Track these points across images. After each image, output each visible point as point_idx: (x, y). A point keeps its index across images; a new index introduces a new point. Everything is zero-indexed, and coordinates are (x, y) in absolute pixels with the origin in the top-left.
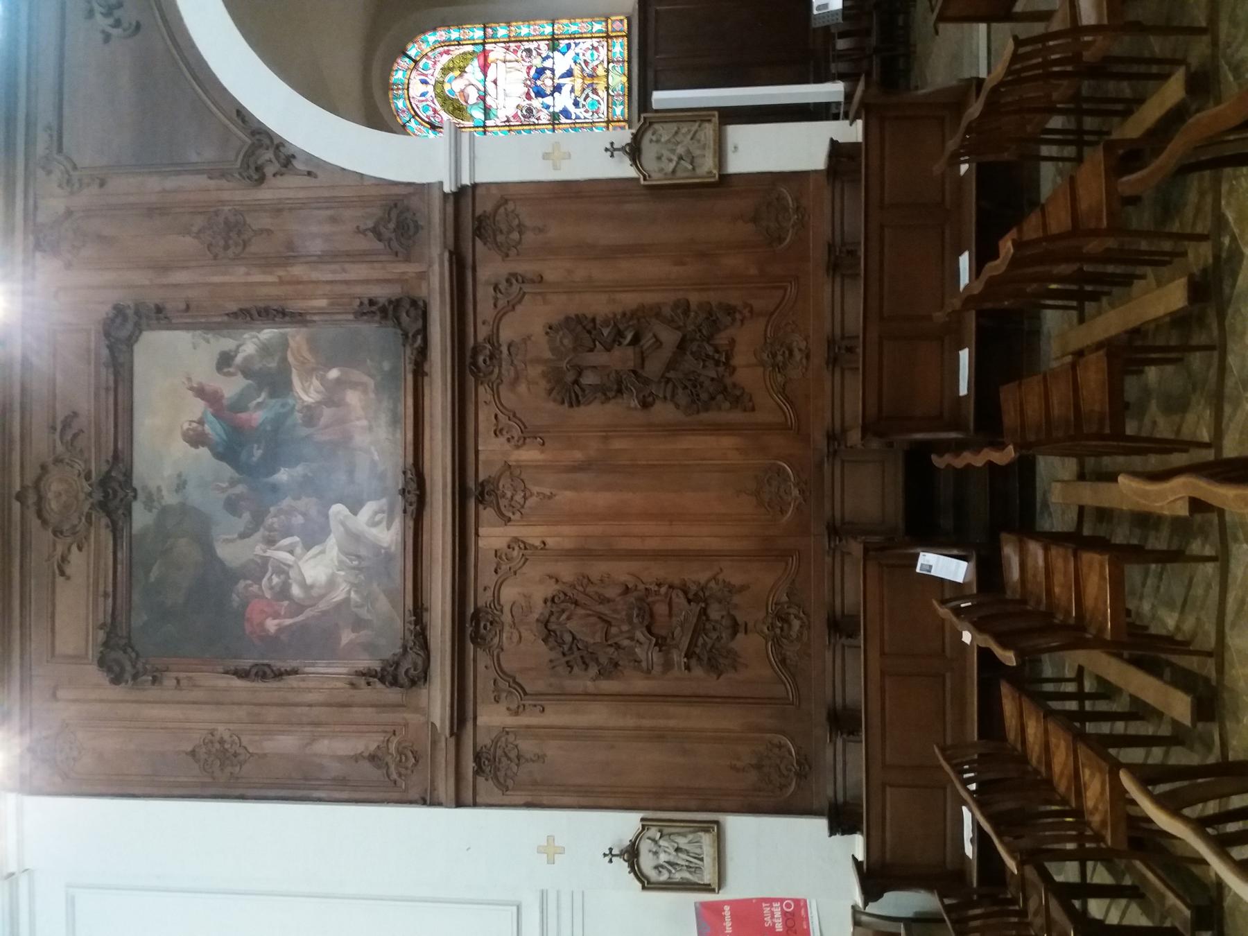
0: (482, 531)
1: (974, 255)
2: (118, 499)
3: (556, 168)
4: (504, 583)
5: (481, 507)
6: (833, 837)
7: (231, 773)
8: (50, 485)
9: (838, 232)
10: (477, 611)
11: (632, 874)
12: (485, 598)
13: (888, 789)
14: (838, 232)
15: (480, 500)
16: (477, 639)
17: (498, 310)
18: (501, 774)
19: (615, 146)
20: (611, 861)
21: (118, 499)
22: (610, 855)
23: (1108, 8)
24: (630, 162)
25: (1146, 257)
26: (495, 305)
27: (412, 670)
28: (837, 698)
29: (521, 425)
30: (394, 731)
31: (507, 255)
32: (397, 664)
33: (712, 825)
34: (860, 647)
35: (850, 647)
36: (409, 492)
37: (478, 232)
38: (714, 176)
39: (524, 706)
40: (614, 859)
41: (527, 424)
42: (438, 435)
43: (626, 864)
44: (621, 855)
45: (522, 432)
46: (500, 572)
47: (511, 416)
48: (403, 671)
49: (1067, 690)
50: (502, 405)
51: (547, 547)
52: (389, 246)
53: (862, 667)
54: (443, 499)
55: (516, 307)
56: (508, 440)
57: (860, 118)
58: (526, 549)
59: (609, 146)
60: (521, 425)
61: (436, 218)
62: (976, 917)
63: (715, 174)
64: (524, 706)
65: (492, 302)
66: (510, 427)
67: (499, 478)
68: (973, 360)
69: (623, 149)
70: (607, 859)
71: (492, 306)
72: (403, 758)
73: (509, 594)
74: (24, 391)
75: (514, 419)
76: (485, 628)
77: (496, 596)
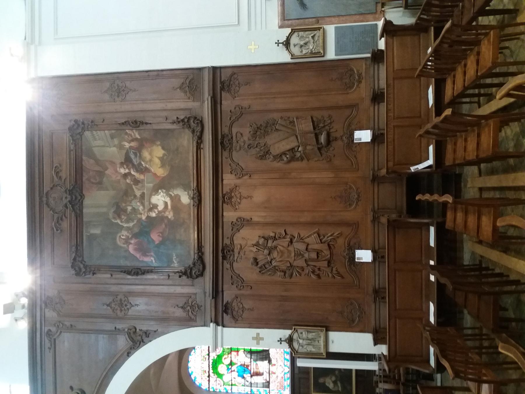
0: (225, 214)
1: (434, 145)
2: (78, 201)
3: (258, 334)
4: (234, 123)
5: (223, 151)
6: (376, 346)
7: (125, 313)
8: (51, 195)
9: (377, 306)
10: (223, 137)
11: (290, 349)
12: (227, 242)
13: (397, 272)
14: (377, 306)
15: (224, 148)
16: (224, 148)
17: (231, 121)
18: (232, 92)
19: (279, 42)
20: (281, 343)
21: (78, 201)
22: (278, 43)
23: (493, 220)
24: (286, 49)
25: (504, 38)
26: (232, 230)
27: (197, 272)
28: (375, 167)
29: (242, 280)
30: (191, 296)
31: (237, 320)
32: (191, 269)
33: (323, 329)
34: (386, 302)
35: (383, 302)
36: (195, 198)
37: (222, 89)
38: (324, 356)
39: (243, 286)
40: (282, 342)
41: (245, 279)
42: (207, 164)
43: (287, 345)
44: (285, 341)
45: (242, 283)
46: (232, 119)
47: (238, 276)
48: (194, 272)
49: (471, 93)
50: (234, 272)
51: (252, 221)
52: (188, 314)
53: (387, 238)
54: (208, 110)
55: (240, 231)
56: (235, 175)
57: (384, 37)
58: (242, 109)
59: (277, 42)
60: (242, 280)
61: (207, 78)
62: (429, 65)
63: (322, 53)
64: (243, 286)
65: (231, 228)
66: (238, 281)
67: (232, 302)
68: (435, 244)
69: (282, 43)
70: (279, 342)
71: (231, 230)
72: (194, 307)
73: (238, 240)
74: (39, 129)
75: (238, 166)
76: (227, 252)
77: (232, 240)
